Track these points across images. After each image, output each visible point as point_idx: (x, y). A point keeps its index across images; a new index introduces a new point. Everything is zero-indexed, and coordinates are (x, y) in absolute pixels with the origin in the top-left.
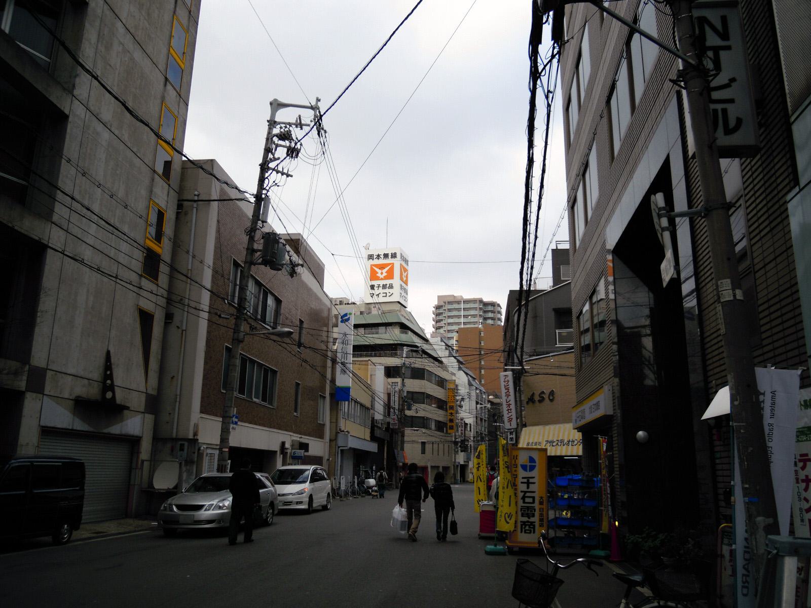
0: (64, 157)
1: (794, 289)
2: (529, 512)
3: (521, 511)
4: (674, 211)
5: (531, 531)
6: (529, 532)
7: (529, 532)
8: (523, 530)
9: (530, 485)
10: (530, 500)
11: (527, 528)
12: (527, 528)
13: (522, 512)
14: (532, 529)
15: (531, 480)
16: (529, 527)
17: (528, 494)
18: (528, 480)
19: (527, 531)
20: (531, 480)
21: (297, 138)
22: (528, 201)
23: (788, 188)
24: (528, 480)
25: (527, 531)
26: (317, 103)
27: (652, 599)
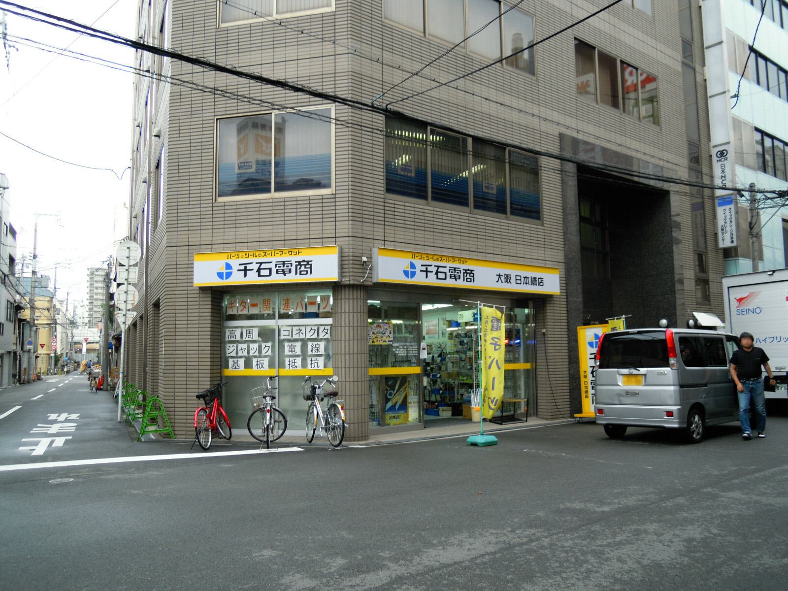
0: (472, 153)
1: (770, 169)
2: (285, 268)
3: (276, 267)
4: (581, 412)
5: (307, 271)
6: (305, 273)
7: (305, 273)
8: (298, 271)
9: (248, 272)
10: (267, 272)
11: (303, 268)
12: (303, 268)
13: (277, 268)
14: (309, 270)
15: (249, 267)
16: (305, 268)
17: (263, 266)
18: (246, 267)
19: (302, 273)
20: (249, 267)
21: (135, 69)
22: (59, 19)
23: (433, 161)
24: (246, 267)
25: (302, 273)
26: (4, 17)
27: (536, 573)
